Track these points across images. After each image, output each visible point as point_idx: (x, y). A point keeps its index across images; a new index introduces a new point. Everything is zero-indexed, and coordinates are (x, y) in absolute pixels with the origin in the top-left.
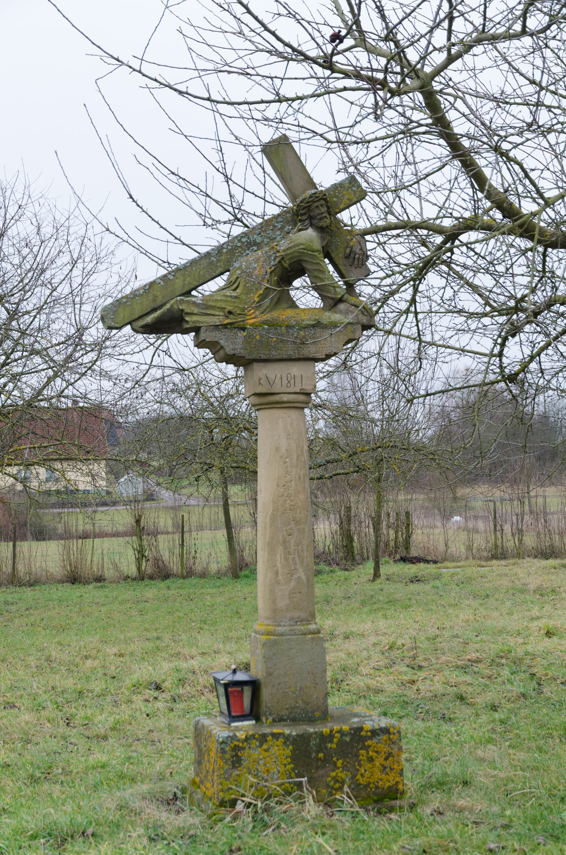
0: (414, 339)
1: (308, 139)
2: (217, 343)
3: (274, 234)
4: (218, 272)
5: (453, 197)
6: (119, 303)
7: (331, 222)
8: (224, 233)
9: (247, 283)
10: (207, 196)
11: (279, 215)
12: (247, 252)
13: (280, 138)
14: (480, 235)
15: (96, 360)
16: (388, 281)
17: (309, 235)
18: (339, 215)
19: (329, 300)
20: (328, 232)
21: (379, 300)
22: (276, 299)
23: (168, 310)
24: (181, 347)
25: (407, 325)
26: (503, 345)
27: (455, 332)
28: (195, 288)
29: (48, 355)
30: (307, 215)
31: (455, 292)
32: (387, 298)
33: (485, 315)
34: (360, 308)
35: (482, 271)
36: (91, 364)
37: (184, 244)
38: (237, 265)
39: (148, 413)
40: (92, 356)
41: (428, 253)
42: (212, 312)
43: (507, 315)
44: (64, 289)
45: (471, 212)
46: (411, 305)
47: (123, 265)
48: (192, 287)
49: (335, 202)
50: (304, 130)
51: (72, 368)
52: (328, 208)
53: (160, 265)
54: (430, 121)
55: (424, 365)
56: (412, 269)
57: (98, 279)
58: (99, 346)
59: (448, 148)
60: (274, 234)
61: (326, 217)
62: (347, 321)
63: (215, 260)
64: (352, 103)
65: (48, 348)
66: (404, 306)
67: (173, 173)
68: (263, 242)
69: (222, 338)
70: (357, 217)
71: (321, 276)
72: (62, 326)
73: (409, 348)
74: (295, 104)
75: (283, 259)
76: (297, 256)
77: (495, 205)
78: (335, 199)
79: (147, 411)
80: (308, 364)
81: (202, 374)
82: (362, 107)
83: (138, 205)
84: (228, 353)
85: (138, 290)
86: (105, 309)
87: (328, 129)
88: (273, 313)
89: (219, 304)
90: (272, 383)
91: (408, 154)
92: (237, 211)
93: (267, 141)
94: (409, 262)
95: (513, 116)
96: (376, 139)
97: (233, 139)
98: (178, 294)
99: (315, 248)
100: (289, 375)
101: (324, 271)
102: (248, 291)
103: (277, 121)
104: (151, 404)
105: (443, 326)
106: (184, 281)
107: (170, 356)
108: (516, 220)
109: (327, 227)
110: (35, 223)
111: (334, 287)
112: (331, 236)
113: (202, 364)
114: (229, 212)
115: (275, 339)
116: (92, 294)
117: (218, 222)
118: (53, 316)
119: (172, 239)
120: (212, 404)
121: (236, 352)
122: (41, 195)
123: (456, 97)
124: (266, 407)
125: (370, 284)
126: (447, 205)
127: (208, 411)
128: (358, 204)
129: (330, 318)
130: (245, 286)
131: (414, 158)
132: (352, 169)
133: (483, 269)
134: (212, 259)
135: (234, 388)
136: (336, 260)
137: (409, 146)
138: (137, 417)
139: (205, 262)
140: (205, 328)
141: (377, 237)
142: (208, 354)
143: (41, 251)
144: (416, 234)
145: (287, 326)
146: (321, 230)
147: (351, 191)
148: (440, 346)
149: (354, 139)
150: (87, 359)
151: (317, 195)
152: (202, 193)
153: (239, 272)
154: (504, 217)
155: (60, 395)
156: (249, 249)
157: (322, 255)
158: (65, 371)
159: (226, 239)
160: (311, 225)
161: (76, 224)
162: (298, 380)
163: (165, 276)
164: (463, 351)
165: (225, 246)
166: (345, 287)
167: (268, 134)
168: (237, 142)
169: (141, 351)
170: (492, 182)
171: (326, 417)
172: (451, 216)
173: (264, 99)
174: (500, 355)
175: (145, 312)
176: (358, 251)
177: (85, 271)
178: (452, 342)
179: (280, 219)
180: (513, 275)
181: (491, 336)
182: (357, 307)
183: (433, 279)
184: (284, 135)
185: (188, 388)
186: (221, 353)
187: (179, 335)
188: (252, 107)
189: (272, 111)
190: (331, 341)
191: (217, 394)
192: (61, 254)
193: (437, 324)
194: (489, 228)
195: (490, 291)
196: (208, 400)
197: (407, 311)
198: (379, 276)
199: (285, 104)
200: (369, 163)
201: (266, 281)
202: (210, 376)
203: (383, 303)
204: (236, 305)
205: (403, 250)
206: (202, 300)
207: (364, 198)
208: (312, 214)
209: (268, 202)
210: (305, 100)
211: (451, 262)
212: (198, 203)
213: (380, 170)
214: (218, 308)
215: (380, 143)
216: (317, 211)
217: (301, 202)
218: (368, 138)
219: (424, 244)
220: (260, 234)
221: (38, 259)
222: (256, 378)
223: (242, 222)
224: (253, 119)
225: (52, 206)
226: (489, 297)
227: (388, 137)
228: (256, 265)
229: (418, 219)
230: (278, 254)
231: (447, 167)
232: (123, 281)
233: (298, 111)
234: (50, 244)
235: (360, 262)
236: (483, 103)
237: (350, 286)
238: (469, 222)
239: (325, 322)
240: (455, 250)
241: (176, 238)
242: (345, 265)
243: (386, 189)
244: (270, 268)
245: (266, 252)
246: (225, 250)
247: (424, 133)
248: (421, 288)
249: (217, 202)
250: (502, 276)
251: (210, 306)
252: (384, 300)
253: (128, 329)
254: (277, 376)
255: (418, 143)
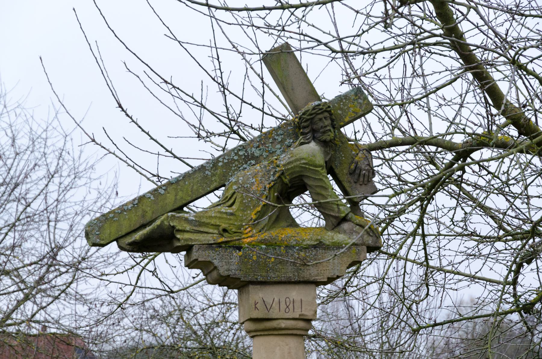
0: (421, 264)
1: (312, 48)
2: (210, 263)
3: (274, 148)
4: (212, 187)
5: (465, 112)
6: (105, 219)
7: (335, 135)
8: (218, 146)
9: (244, 199)
10: (203, 106)
11: (279, 127)
12: (245, 166)
13: (282, 46)
14: (495, 152)
15: (71, 283)
16: (394, 200)
17: (311, 150)
18: (342, 130)
19: (331, 219)
20: (332, 146)
21: (383, 221)
22: (274, 217)
23: (158, 226)
24: (170, 266)
25: (414, 248)
26: (517, 272)
27: (465, 257)
28: (186, 205)
29: (18, 276)
30: (310, 128)
31: (466, 213)
32: (392, 219)
33: (499, 239)
34: (367, 227)
35: (495, 191)
36: (64, 287)
37: (175, 157)
38: (233, 179)
39: (125, 342)
40: (67, 278)
41: (436, 172)
42: (206, 230)
43: (522, 239)
44: (37, 205)
45: (484, 130)
46: (418, 227)
47: (103, 180)
48: (184, 202)
49: (340, 115)
50: (306, 38)
51: (45, 291)
52: (332, 120)
53: (148, 179)
54: (441, 32)
55: (431, 292)
56: (419, 188)
57: (75, 196)
58: (75, 266)
59: (461, 61)
60: (274, 148)
61: (330, 130)
62: (351, 242)
63: (210, 173)
64: (357, 12)
65: (19, 268)
66: (410, 228)
67: (166, 82)
68: (261, 155)
69: (216, 258)
70: (362, 132)
71: (323, 192)
72: (35, 246)
73: (416, 273)
74: (299, 13)
75: (283, 174)
76: (298, 172)
77: (510, 121)
78: (340, 112)
79: (124, 339)
80: (308, 289)
81: (185, 299)
82: (368, 16)
83: (127, 115)
84: (222, 274)
85: (126, 204)
86: (90, 225)
87: (332, 39)
88: (272, 232)
89: (213, 222)
90: (269, 307)
91: (417, 66)
92: (233, 123)
93: (268, 49)
94: (416, 180)
95: (528, 28)
96: (384, 50)
97: (231, 47)
98: (169, 209)
99: (317, 162)
100: (288, 300)
101: (327, 187)
102: (245, 207)
103: (280, 28)
104: (130, 331)
105: (452, 250)
106: (176, 196)
107: (157, 277)
108: (534, 137)
109: (331, 141)
110: (10, 135)
111: (338, 205)
112: (335, 151)
113: (186, 289)
114: (225, 124)
115: (273, 260)
116: (68, 211)
117: (213, 134)
118: (27, 234)
119: (162, 151)
120: (195, 333)
121: (230, 273)
122: (17, 105)
123: (469, 8)
124: (262, 333)
125: (374, 204)
126: (457, 121)
127: (190, 340)
128: (363, 118)
129: (333, 238)
130: (241, 202)
131: (423, 70)
132: (356, 81)
133: (496, 189)
134: (207, 172)
135: (221, 315)
136: (340, 176)
137: (418, 57)
138: (115, 345)
139: (199, 176)
140: (197, 247)
141: (383, 154)
142: (198, 275)
143: (15, 164)
144: (424, 151)
145: (286, 246)
146: (325, 144)
147: (357, 103)
148: (448, 272)
149: (360, 49)
150: (60, 281)
151: (321, 107)
152: (196, 103)
153: (235, 187)
154: (520, 134)
155: (31, 319)
156: (246, 163)
157: (325, 170)
158: (37, 293)
159: (222, 153)
160: (314, 138)
161: (54, 136)
162: (297, 305)
163: (155, 190)
164: (473, 278)
165: (221, 159)
166: (349, 206)
167: (267, 43)
168: (234, 49)
169: (126, 271)
170: (509, 98)
171: (320, 349)
172: (464, 132)
173: (266, 6)
174: (515, 283)
175: (133, 229)
176: (363, 167)
177: (62, 186)
178: (462, 268)
179: (280, 132)
180: (528, 197)
181: (505, 262)
182: (362, 227)
183: (441, 198)
184: (287, 43)
185: (170, 314)
186: (215, 274)
187: (168, 255)
188: (253, 14)
189: (274, 17)
190: (334, 264)
191: (202, 322)
192: (37, 167)
193: (446, 247)
194: (502, 145)
195: (505, 214)
196: (191, 328)
197: (414, 234)
198: (387, 194)
199: (287, 13)
200: (376, 75)
201: (264, 197)
202: (194, 301)
203: (388, 224)
204: (231, 222)
205: (408, 167)
206: (195, 216)
207: (370, 111)
208: (315, 127)
209: (267, 114)
210: (310, 8)
211: (462, 182)
212: (191, 114)
213: (387, 82)
214: (212, 225)
215: (387, 54)
216: (321, 124)
217: (304, 114)
218: (375, 48)
219: (432, 161)
220: (258, 147)
221: (12, 172)
222: (252, 302)
223: (238, 134)
224: (253, 25)
225: (28, 116)
226: (503, 221)
227: (395, 47)
228: (254, 180)
229: (426, 135)
230: (278, 169)
231: (459, 80)
232: (102, 198)
233: (301, 19)
234: (26, 157)
235: (366, 179)
236: (497, 15)
237: (355, 205)
238: (482, 138)
239: (327, 243)
240: (466, 168)
241: (167, 151)
242: (350, 182)
243: (392, 103)
244: (269, 184)
245: (265, 167)
246: (220, 164)
247: (435, 44)
248: (430, 208)
249: (212, 113)
250: (518, 197)
251: (203, 223)
252: (389, 221)
253: (113, 247)
254: (275, 300)
255: (428, 55)
